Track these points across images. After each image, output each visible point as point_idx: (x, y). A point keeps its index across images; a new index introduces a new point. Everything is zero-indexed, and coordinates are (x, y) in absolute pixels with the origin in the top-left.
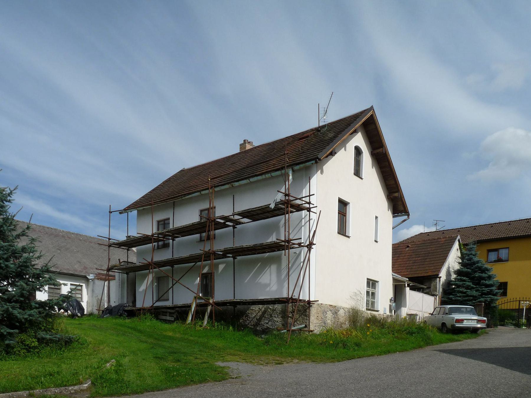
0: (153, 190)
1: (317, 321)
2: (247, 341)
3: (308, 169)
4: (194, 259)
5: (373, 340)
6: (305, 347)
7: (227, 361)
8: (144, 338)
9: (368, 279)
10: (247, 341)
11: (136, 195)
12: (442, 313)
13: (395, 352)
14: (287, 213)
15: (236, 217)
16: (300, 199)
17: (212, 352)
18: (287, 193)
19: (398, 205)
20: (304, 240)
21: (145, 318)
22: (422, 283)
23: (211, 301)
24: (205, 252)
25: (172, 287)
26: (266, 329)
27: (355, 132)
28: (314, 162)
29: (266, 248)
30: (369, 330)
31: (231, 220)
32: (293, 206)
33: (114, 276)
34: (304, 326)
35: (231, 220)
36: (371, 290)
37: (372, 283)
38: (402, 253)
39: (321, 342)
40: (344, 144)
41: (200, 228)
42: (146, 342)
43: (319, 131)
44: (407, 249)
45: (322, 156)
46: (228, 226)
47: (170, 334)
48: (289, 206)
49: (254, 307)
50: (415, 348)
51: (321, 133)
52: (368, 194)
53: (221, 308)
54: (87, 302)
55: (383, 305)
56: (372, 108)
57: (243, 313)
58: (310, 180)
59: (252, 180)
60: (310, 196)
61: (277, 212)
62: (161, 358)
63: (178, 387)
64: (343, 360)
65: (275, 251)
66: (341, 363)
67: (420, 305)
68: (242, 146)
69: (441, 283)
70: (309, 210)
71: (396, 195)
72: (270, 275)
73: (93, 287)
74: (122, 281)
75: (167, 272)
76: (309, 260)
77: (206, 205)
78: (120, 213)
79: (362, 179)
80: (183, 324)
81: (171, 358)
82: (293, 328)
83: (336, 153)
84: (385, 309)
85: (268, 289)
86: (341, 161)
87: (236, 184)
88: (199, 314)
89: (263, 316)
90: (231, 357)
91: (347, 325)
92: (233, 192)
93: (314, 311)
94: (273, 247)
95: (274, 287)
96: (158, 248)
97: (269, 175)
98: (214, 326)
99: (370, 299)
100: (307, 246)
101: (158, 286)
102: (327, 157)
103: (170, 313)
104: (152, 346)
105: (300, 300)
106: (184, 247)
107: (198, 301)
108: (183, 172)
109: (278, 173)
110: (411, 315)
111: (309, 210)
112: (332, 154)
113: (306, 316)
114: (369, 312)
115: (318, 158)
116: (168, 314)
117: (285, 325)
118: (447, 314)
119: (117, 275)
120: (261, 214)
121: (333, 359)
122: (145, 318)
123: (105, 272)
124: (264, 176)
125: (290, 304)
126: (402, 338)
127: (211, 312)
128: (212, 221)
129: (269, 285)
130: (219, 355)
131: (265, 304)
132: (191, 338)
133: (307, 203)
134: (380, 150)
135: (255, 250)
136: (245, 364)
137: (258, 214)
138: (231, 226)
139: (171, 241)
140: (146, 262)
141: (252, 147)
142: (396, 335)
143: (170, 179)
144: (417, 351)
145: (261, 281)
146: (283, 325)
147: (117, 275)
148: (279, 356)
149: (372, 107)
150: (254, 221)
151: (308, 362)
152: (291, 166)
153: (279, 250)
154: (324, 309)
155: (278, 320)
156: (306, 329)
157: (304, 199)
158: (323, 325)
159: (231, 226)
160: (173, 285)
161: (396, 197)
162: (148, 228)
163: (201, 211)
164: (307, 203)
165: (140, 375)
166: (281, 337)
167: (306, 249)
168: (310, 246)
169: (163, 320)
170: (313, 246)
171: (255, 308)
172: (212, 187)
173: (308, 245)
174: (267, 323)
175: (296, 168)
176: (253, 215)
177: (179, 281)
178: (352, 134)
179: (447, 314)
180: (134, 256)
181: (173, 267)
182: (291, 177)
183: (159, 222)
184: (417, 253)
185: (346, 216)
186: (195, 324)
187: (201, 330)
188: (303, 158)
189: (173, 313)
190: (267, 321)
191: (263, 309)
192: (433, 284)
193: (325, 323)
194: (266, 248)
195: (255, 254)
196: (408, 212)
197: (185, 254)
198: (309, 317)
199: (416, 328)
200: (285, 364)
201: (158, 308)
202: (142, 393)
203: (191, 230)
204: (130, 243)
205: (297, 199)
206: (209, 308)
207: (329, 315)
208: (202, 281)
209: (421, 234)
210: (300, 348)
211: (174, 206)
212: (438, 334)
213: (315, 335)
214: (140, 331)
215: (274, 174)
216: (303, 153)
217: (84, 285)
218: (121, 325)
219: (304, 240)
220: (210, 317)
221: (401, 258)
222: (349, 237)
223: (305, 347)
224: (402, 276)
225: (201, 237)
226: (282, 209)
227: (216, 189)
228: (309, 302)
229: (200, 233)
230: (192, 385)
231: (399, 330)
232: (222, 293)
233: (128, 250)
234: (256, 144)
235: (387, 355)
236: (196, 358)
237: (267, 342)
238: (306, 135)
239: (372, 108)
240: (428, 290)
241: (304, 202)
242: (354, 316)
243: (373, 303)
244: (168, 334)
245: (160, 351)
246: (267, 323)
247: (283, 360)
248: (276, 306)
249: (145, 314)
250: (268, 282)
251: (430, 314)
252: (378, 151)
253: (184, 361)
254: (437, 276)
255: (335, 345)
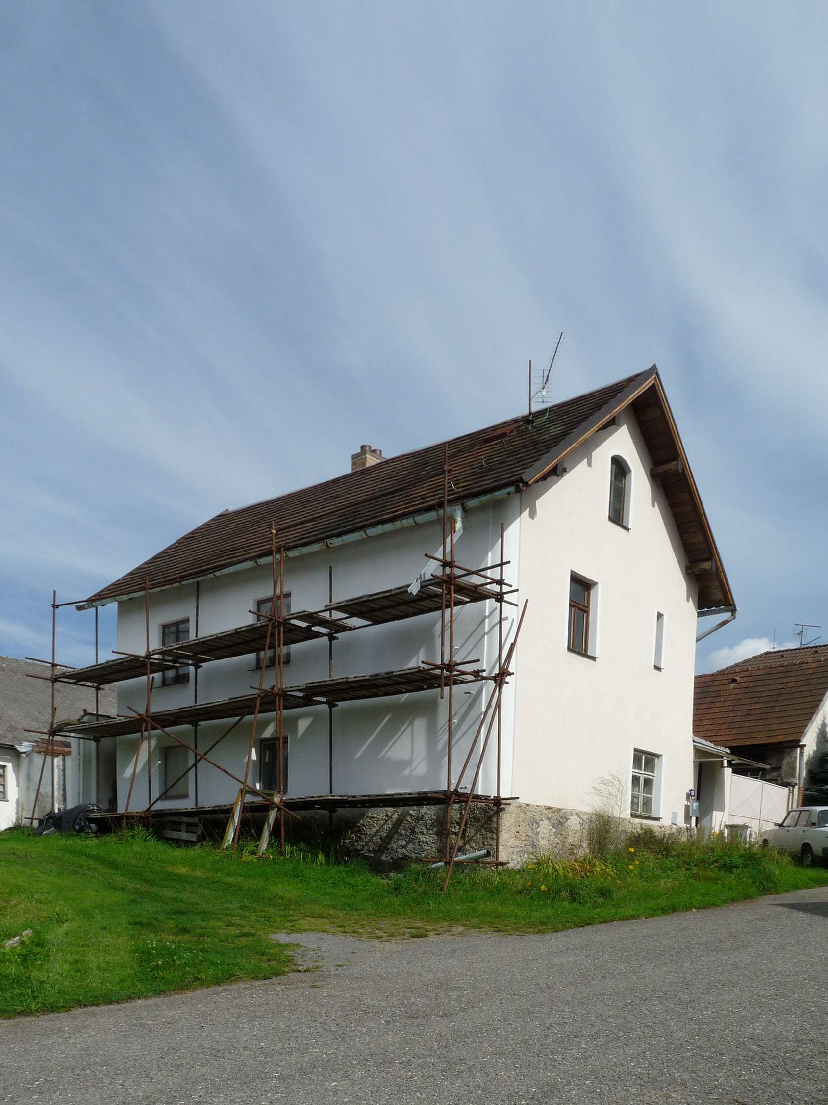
0: (155, 558)
1: (517, 843)
2: (353, 886)
3: (499, 506)
4: (240, 708)
5: (641, 884)
6: (481, 899)
7: (300, 931)
8: (119, 879)
9: (636, 750)
10: (353, 886)
11: (117, 569)
12: (803, 821)
13: (687, 909)
14: (448, 606)
15: (337, 615)
16: (477, 573)
17: (271, 910)
18: (448, 559)
19: (709, 587)
20: (488, 665)
21: (133, 837)
22: (761, 759)
23: (276, 799)
24: (265, 691)
25: (195, 765)
26: (402, 859)
27: (613, 423)
28: (512, 489)
29: (402, 683)
30: (633, 860)
31: (323, 623)
32: (461, 589)
33: (68, 745)
34: (484, 852)
35: (323, 623)
36: (643, 774)
37: (645, 759)
38: (715, 695)
39: (520, 887)
40: (585, 451)
41: (254, 640)
42: (122, 889)
43: (532, 422)
44: (733, 686)
45: (531, 475)
46: (318, 635)
47: (183, 870)
48: (454, 590)
49: (373, 812)
50: (734, 900)
51: (533, 428)
52: (642, 561)
53: (297, 815)
54: (18, 801)
55: (671, 807)
56: (653, 370)
57: (351, 825)
58: (503, 530)
59: (371, 532)
60: (502, 564)
61: (426, 603)
62: (148, 926)
63: (158, 993)
64: (565, 928)
65: (422, 689)
66: (559, 934)
67: (756, 806)
68: (358, 458)
69: (805, 758)
70: (499, 598)
71: (707, 565)
72: (412, 741)
73: (29, 769)
74: (85, 756)
75: (185, 735)
76: (498, 705)
77: (265, 591)
78: (79, 608)
79: (627, 529)
80: (215, 848)
81: (171, 924)
82: (461, 857)
83: (565, 470)
84: (675, 815)
85: (407, 772)
86: (579, 490)
87: (336, 542)
88: (251, 827)
89: (396, 832)
90: (312, 920)
91: (584, 851)
92: (329, 562)
93: (508, 821)
94: (417, 681)
95: (420, 768)
96: (164, 684)
97: (411, 520)
98: (282, 853)
99: (642, 795)
100: (494, 678)
101: (165, 769)
102: (544, 478)
103: (189, 825)
104: (133, 897)
105: (477, 797)
106: (221, 681)
107: (249, 798)
108: (224, 519)
109: (431, 516)
110: (732, 828)
111: (499, 598)
112: (557, 472)
113: (491, 831)
114: (637, 821)
115: (521, 480)
116: (183, 828)
117: (444, 852)
118: (814, 824)
119: (74, 742)
120: (391, 607)
121: (544, 926)
122: (133, 837)
123: (46, 737)
124: (398, 524)
125: (456, 806)
126: (707, 879)
127: (277, 821)
128: (280, 623)
129: (409, 763)
130: (284, 916)
131: (398, 806)
132: (229, 880)
133: (494, 581)
134: (672, 465)
135: (376, 686)
136: (340, 938)
137: (383, 608)
138: (323, 635)
139: (192, 668)
140: (134, 715)
141: (379, 461)
142: (695, 870)
143: (193, 533)
144: (739, 907)
145: (389, 754)
146: (440, 851)
147: (74, 742)
148: (421, 919)
149: (654, 368)
150: (376, 622)
151: (486, 933)
152: (459, 499)
153: (431, 687)
154: (532, 817)
155: (429, 840)
156: (489, 859)
157: (489, 573)
158: (531, 850)
159: (323, 635)
160: (197, 761)
161: (705, 570)
162: (141, 639)
163: (260, 603)
164: (494, 581)
165: (79, 967)
166: (428, 876)
167: (492, 684)
168: (500, 678)
169: (173, 839)
170: (508, 679)
171: (378, 814)
172: (278, 551)
173: (497, 675)
174: (404, 847)
175: (472, 503)
176: (374, 610)
177: (206, 757)
178: (604, 427)
179: (814, 824)
180: (110, 703)
181: (195, 725)
182: (459, 525)
183: (165, 627)
184: (754, 695)
185: (587, 612)
186: (241, 850)
187: (252, 861)
188: (488, 483)
189: (196, 825)
190: (404, 843)
191: (396, 816)
192: (787, 760)
193: (534, 846)
194: (402, 683)
195: (377, 695)
196: (733, 604)
197: (220, 697)
198: (497, 834)
199: (741, 856)
200: (432, 938)
201: (160, 814)
202: (66, 1008)
203: (235, 645)
204: (99, 676)
205: (470, 573)
206: (272, 815)
207: (545, 828)
208: (260, 755)
209: (766, 653)
210: (472, 902)
211: (198, 591)
212: (791, 868)
213: (511, 872)
214: (114, 865)
215: (421, 518)
216: (491, 470)
217: (9, 765)
218: (74, 852)
219: (488, 665)
220: (275, 833)
221: (717, 704)
222: (593, 658)
223: (481, 899)
224: (716, 743)
225: (258, 660)
226: (437, 595)
227: (292, 554)
228: (497, 801)
229: (257, 650)
230: (195, 989)
231: (703, 861)
232: (305, 781)
233: (98, 689)
234: (389, 453)
235: (669, 917)
236: (230, 925)
237: (397, 889)
238: (499, 432)
239: (653, 370)
240: (774, 774)
241: (489, 581)
242: (601, 830)
243: (647, 803)
244: (176, 871)
245: (148, 909)
246: (404, 847)
247: (428, 928)
248: (424, 809)
249: (132, 828)
250: (407, 757)
251: (776, 825)
252: (666, 467)
253: (198, 931)
254: (795, 744)
255: (552, 895)
